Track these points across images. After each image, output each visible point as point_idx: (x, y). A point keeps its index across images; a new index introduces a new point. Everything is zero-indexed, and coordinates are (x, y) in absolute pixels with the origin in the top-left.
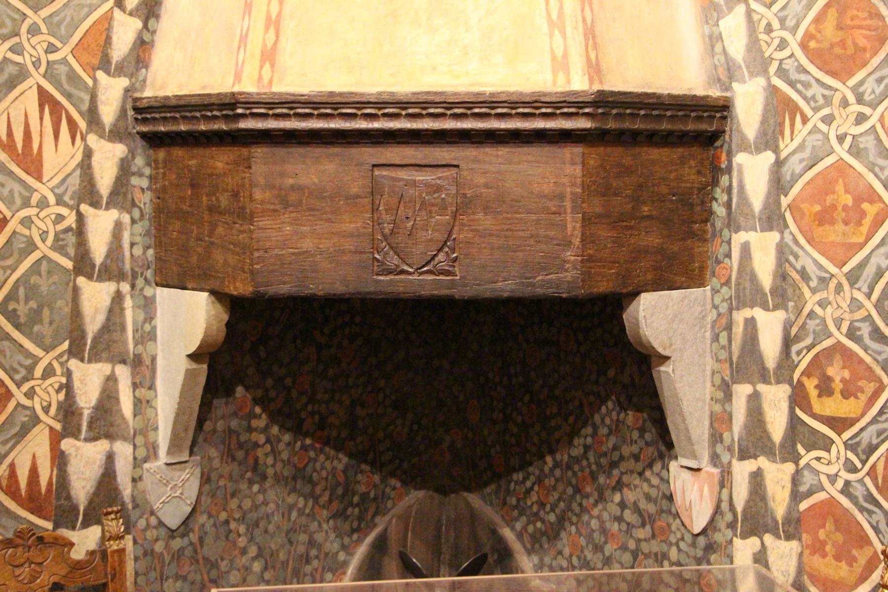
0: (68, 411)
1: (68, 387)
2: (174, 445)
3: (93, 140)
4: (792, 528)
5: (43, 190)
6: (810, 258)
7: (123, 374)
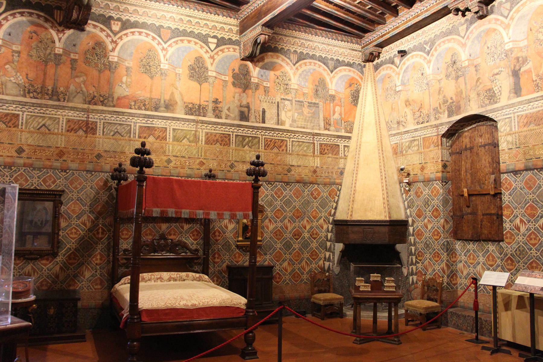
0: (325, 258)
4: (416, 274)
5: (323, 231)
6: (417, 240)
7: (331, 254)
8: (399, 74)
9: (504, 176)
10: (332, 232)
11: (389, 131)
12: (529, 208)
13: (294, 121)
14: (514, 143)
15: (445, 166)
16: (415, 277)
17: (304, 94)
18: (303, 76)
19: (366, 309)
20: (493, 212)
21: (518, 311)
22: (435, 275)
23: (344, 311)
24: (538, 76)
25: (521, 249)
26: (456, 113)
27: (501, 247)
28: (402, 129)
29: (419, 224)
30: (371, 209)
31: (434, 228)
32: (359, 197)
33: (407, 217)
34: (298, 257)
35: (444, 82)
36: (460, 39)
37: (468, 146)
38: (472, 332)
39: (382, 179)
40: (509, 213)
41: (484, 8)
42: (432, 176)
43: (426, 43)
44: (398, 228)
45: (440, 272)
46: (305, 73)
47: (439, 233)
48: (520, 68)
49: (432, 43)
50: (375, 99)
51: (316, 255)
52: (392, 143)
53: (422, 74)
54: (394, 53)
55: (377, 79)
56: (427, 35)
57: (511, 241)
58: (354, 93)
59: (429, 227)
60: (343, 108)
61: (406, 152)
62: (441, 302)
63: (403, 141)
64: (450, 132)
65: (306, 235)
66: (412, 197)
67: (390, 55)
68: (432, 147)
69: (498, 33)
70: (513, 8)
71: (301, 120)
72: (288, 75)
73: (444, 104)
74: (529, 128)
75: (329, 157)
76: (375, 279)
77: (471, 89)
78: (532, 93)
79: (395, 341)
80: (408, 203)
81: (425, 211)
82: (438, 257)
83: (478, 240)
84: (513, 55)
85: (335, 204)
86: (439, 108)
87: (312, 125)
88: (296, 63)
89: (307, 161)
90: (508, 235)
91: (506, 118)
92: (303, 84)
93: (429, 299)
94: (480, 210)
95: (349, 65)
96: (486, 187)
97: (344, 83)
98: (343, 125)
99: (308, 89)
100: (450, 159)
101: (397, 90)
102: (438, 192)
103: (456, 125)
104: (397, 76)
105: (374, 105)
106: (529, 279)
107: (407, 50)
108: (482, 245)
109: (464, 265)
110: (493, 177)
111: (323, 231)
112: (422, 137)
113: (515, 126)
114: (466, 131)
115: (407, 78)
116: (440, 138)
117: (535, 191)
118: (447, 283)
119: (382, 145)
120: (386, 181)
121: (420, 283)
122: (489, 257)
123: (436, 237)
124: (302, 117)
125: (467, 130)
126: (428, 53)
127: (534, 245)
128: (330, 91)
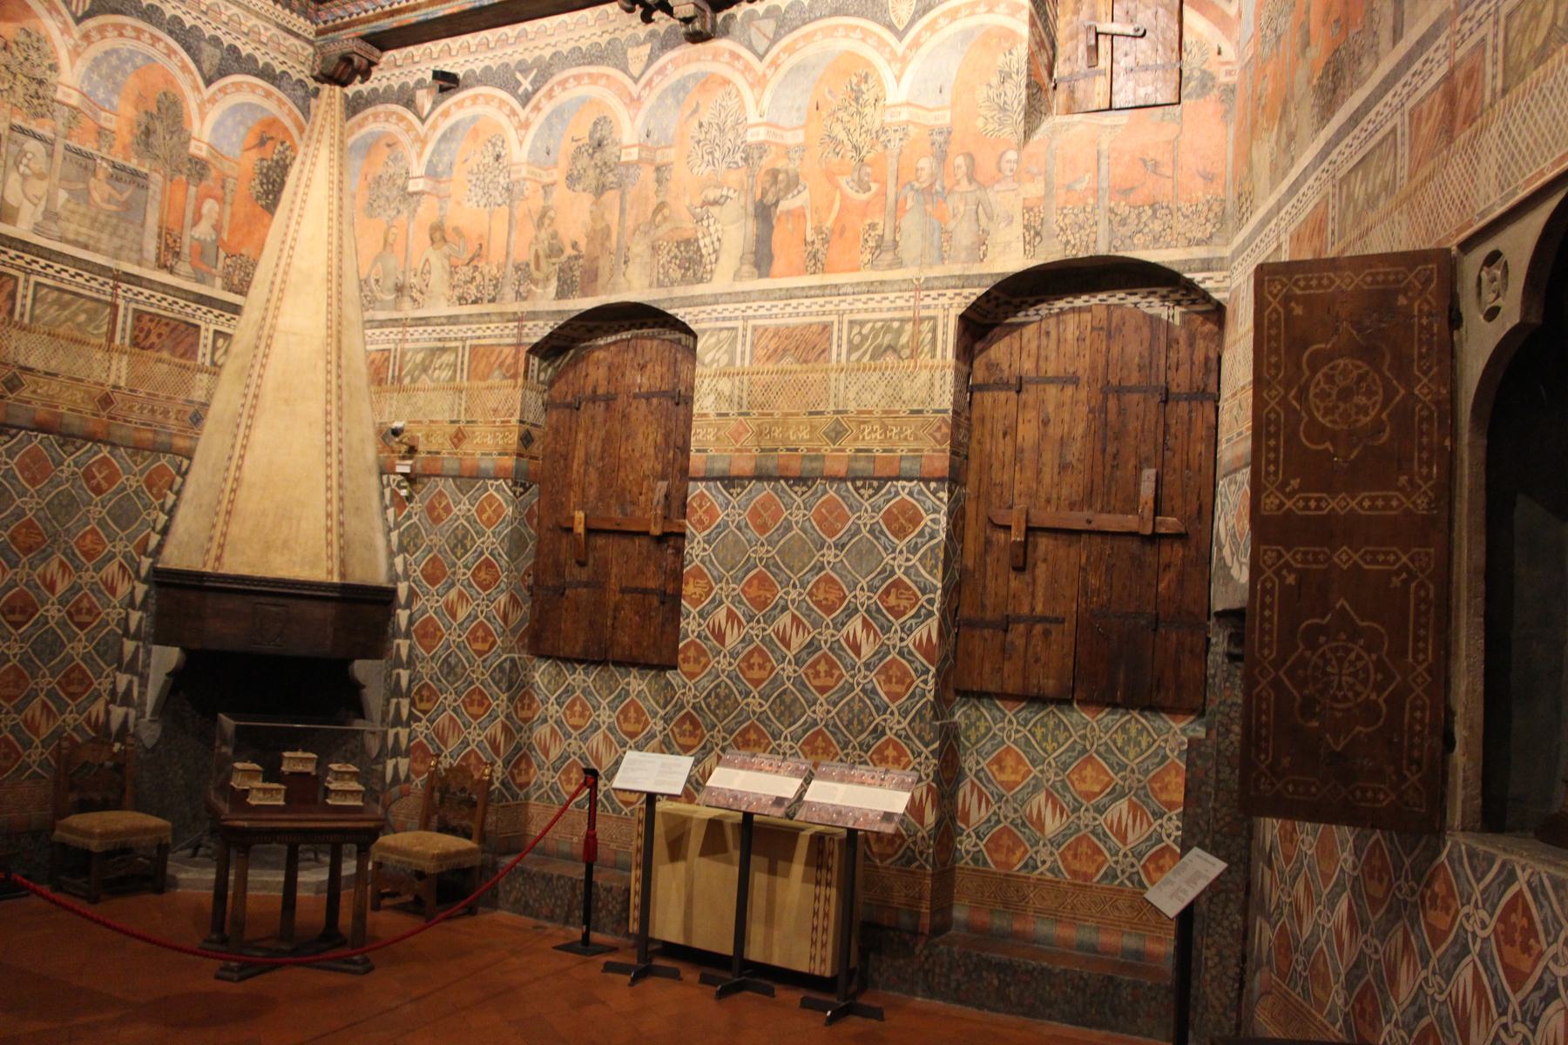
0: (113, 692)
1: (114, 683)
2: (154, 713)
3: (136, 583)
4: (407, 753)
5: (116, 602)
6: (420, 650)
7: (136, 680)
8: (423, 142)
9: (696, 489)
10: (144, 606)
11: (364, 308)
12: (755, 582)
13: (51, 215)
14: (736, 399)
15: (526, 439)
16: (404, 764)
17: (101, 132)
18: (104, 69)
19: (265, 865)
20: (652, 584)
21: (703, 860)
22: (465, 758)
23: (170, 871)
24: (818, 230)
25: (722, 691)
26: (582, 289)
27: (669, 683)
28: (408, 311)
29: (431, 603)
30: (285, 542)
31: (476, 617)
32: (249, 501)
33: (395, 578)
34: (17, 686)
35: (561, 193)
36: (628, 81)
37: (600, 391)
38: (566, 922)
39: (329, 454)
40: (698, 591)
41: (709, 14)
42: (487, 464)
43: (524, 68)
44: (363, 610)
45: (484, 750)
46: (114, 60)
47: (488, 633)
48: (777, 202)
49: (544, 71)
50: (335, 202)
51: (81, 682)
52: (369, 347)
53: (498, 157)
54: (419, 75)
55: (350, 141)
56: (531, 45)
57: (697, 668)
58: (269, 168)
59: (462, 614)
60: (228, 210)
61: (414, 380)
62: (483, 839)
63: (407, 346)
64: (555, 343)
65: (53, 612)
66: (415, 519)
67: (403, 79)
68: (496, 379)
69: (734, 92)
70: (781, 37)
71: (77, 217)
72: (48, 48)
73: (549, 256)
74: (779, 366)
75: (160, 360)
76: (300, 768)
77: (637, 228)
78: (799, 274)
79: (355, 963)
80: (401, 535)
81: (454, 565)
82: (481, 704)
83: (601, 662)
84: (763, 162)
85: (163, 518)
86: (532, 266)
87: (117, 242)
88: (88, 15)
89: (81, 362)
90: (692, 653)
91: (721, 329)
92: (101, 94)
93: (444, 829)
94: (617, 574)
95: (267, 74)
96: (639, 513)
97: (242, 130)
98: (220, 266)
99: (120, 117)
100: (542, 421)
101: (411, 189)
102: (498, 512)
103: (577, 324)
104: (418, 145)
105: (330, 219)
106: (743, 773)
107: (461, 76)
108: (612, 675)
109: (553, 732)
110: (662, 486)
111: (116, 602)
112: (468, 343)
113: (743, 353)
114: (600, 348)
115: (446, 159)
116: (522, 356)
117: (776, 538)
118: (503, 783)
119: (339, 349)
120: (340, 463)
121: (419, 782)
122: (630, 712)
123: (479, 646)
124: (82, 209)
125: (608, 348)
126: (525, 99)
127: (757, 682)
128: (193, 143)
